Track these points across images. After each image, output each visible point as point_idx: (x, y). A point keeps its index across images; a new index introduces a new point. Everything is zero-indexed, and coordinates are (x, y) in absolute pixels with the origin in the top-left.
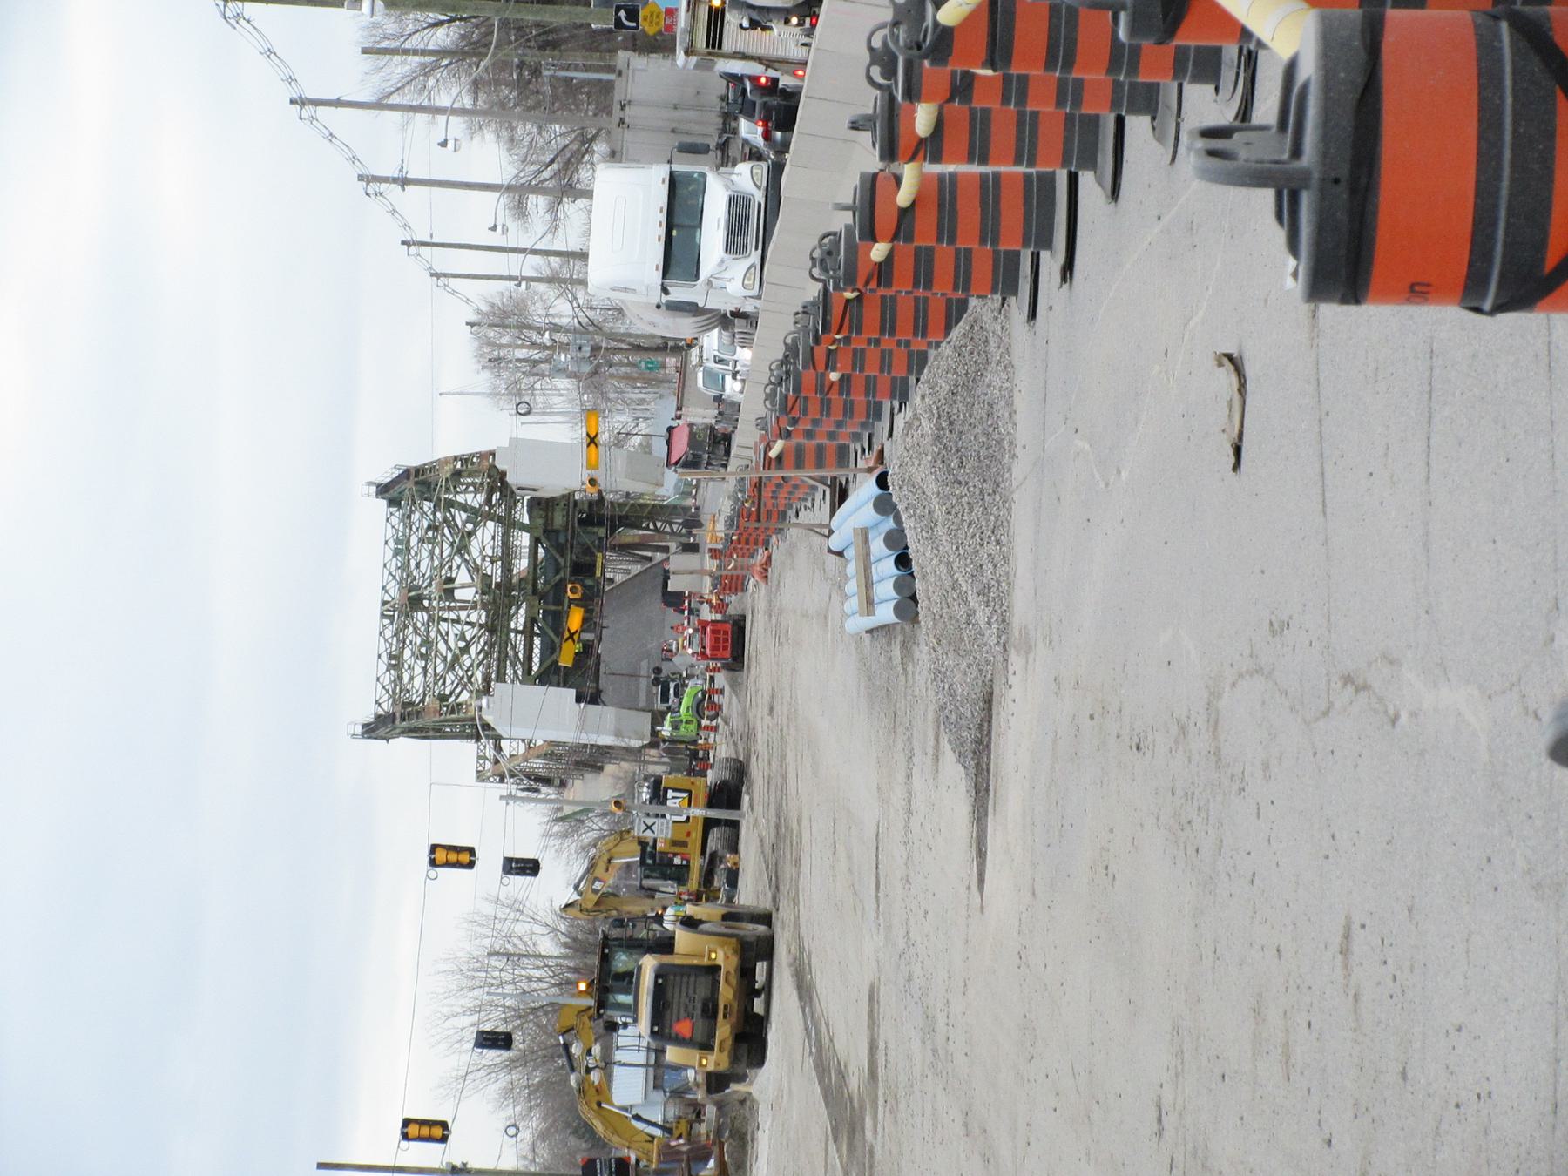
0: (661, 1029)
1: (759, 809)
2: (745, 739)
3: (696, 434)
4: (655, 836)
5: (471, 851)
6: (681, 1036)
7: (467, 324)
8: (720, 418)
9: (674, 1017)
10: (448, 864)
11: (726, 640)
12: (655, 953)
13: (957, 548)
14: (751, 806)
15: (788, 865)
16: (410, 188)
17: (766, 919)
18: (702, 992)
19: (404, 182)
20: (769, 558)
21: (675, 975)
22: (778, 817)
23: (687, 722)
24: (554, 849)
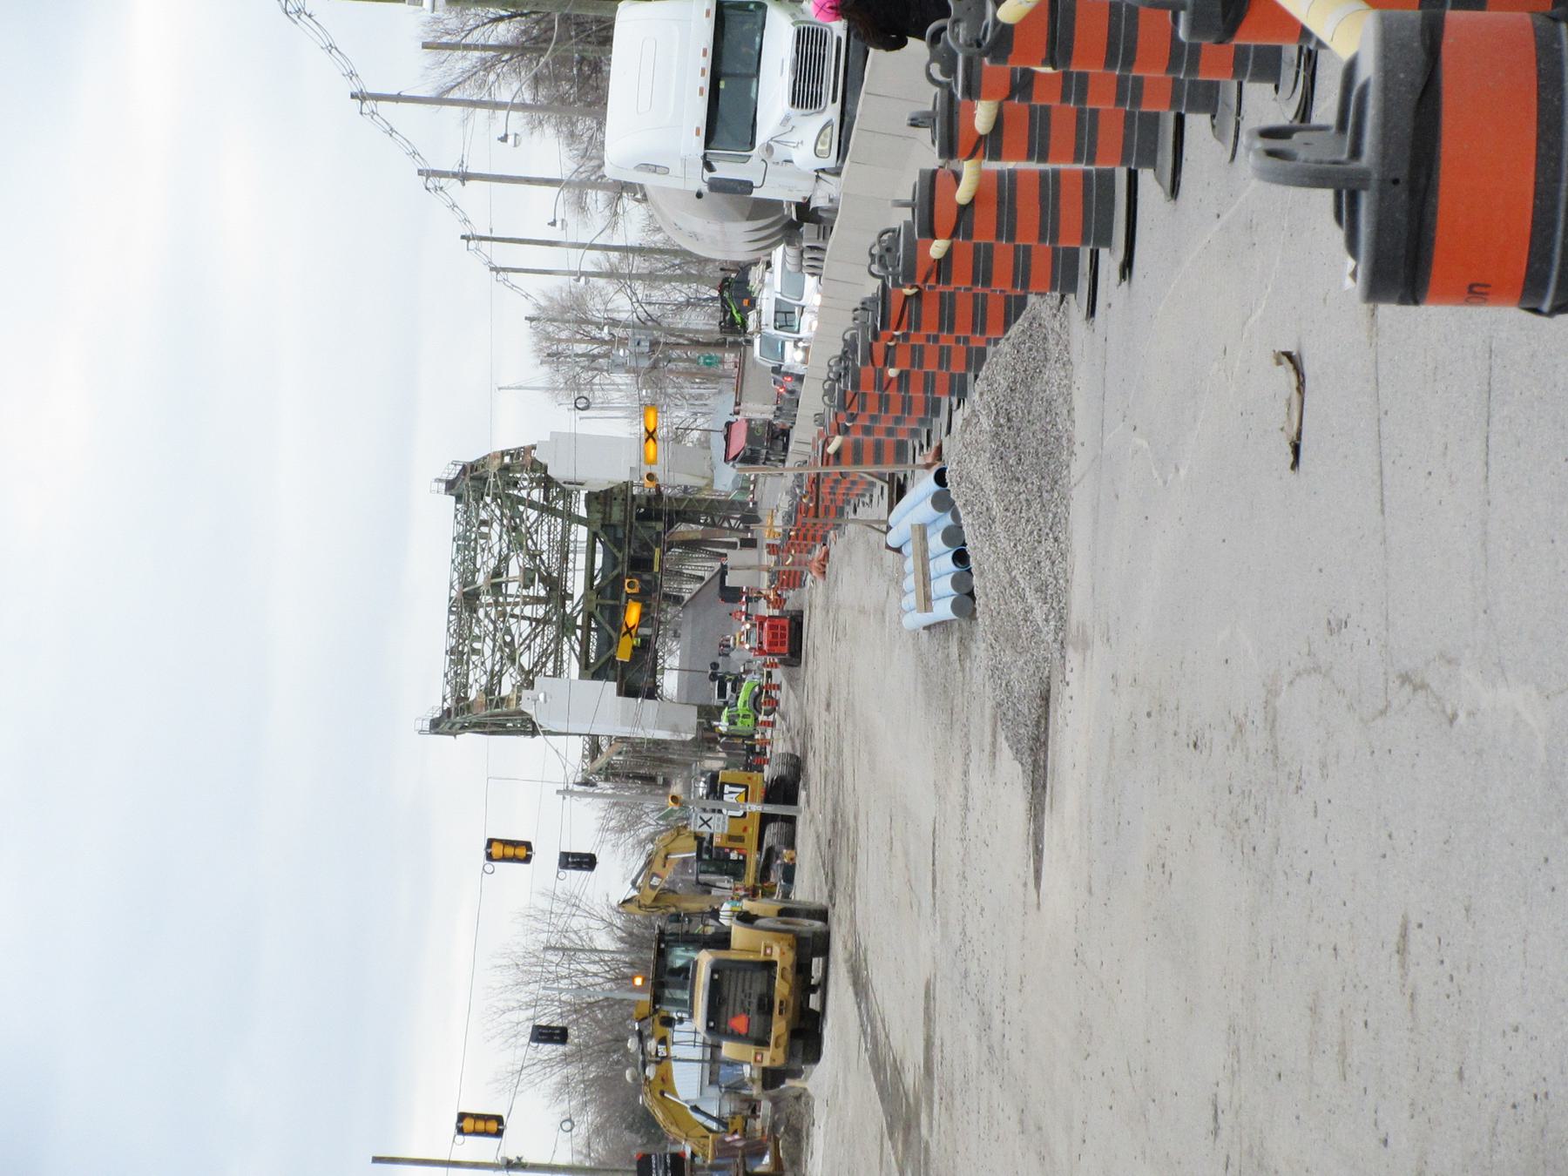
0: (717, 1024)
1: (815, 804)
3: (754, 429)
5: (528, 846)
6: (736, 1031)
8: (778, 413)
9: (730, 1014)
10: (504, 859)
11: (783, 636)
12: (710, 948)
13: (1015, 545)
17: (822, 915)
18: (758, 987)
19: (465, 177)
20: (827, 554)
22: (835, 811)
24: (610, 843)
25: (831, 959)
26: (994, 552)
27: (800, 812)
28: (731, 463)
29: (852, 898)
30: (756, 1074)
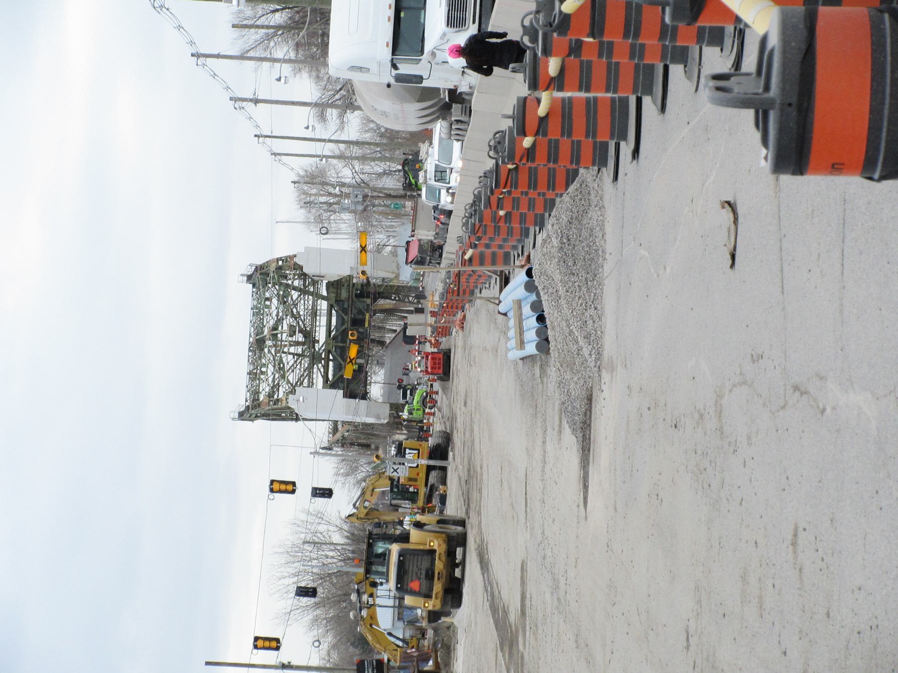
1: (458, 459)
2: (450, 420)
3: (422, 245)
4: (399, 475)
5: (294, 484)
8: (436, 236)
9: (410, 579)
10: (280, 491)
13: (572, 312)
14: (454, 458)
15: (475, 493)
16: (259, 105)
17: (462, 523)
18: (425, 564)
19: (256, 101)
22: (469, 465)
23: (417, 410)
25: (467, 549)
26: (560, 316)
27: (449, 464)
28: (410, 265)
29: (479, 514)
30: (425, 614)
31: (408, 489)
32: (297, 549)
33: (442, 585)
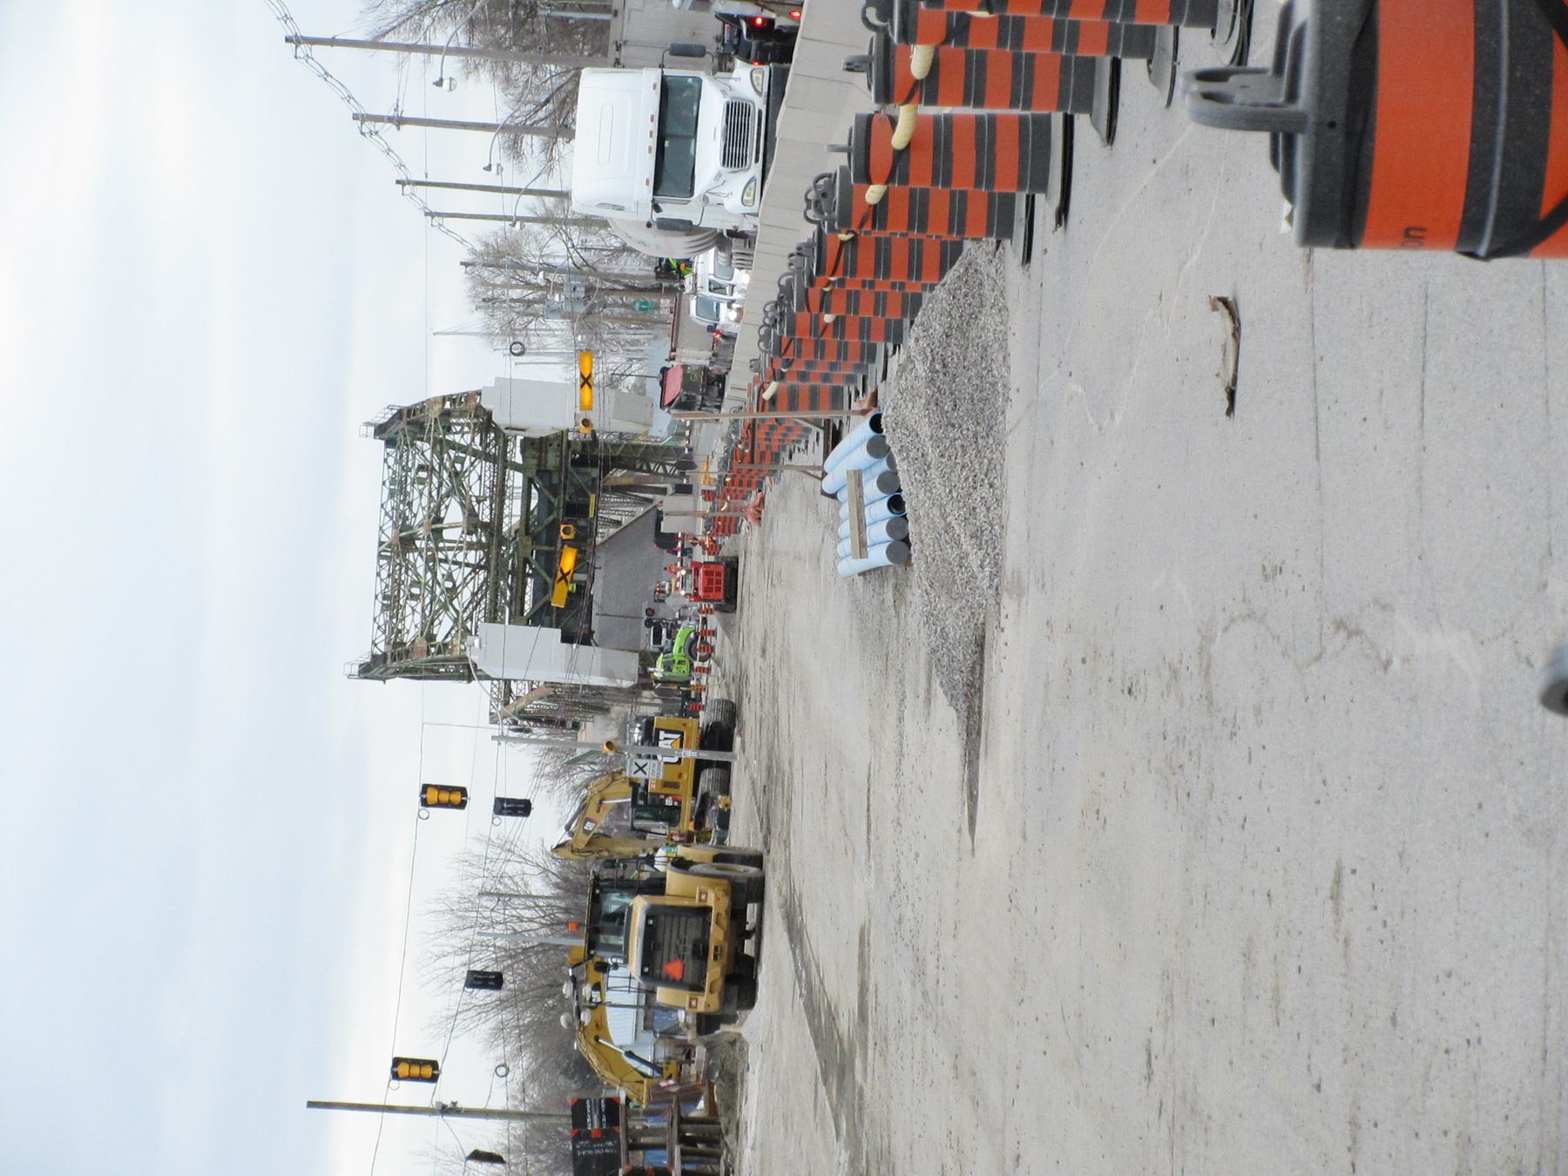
1: (750, 749)
5: (463, 791)
6: (671, 977)
7: (462, 263)
8: (714, 359)
9: (665, 957)
10: (439, 804)
11: (718, 582)
13: (951, 491)
17: (757, 860)
18: (693, 933)
19: (399, 121)
20: (762, 500)
21: (666, 916)
25: (766, 905)
26: (929, 499)
27: (735, 758)
28: (667, 410)
29: (787, 844)
30: (691, 1020)
31: (663, 801)
32: (467, 905)
33: (722, 968)
